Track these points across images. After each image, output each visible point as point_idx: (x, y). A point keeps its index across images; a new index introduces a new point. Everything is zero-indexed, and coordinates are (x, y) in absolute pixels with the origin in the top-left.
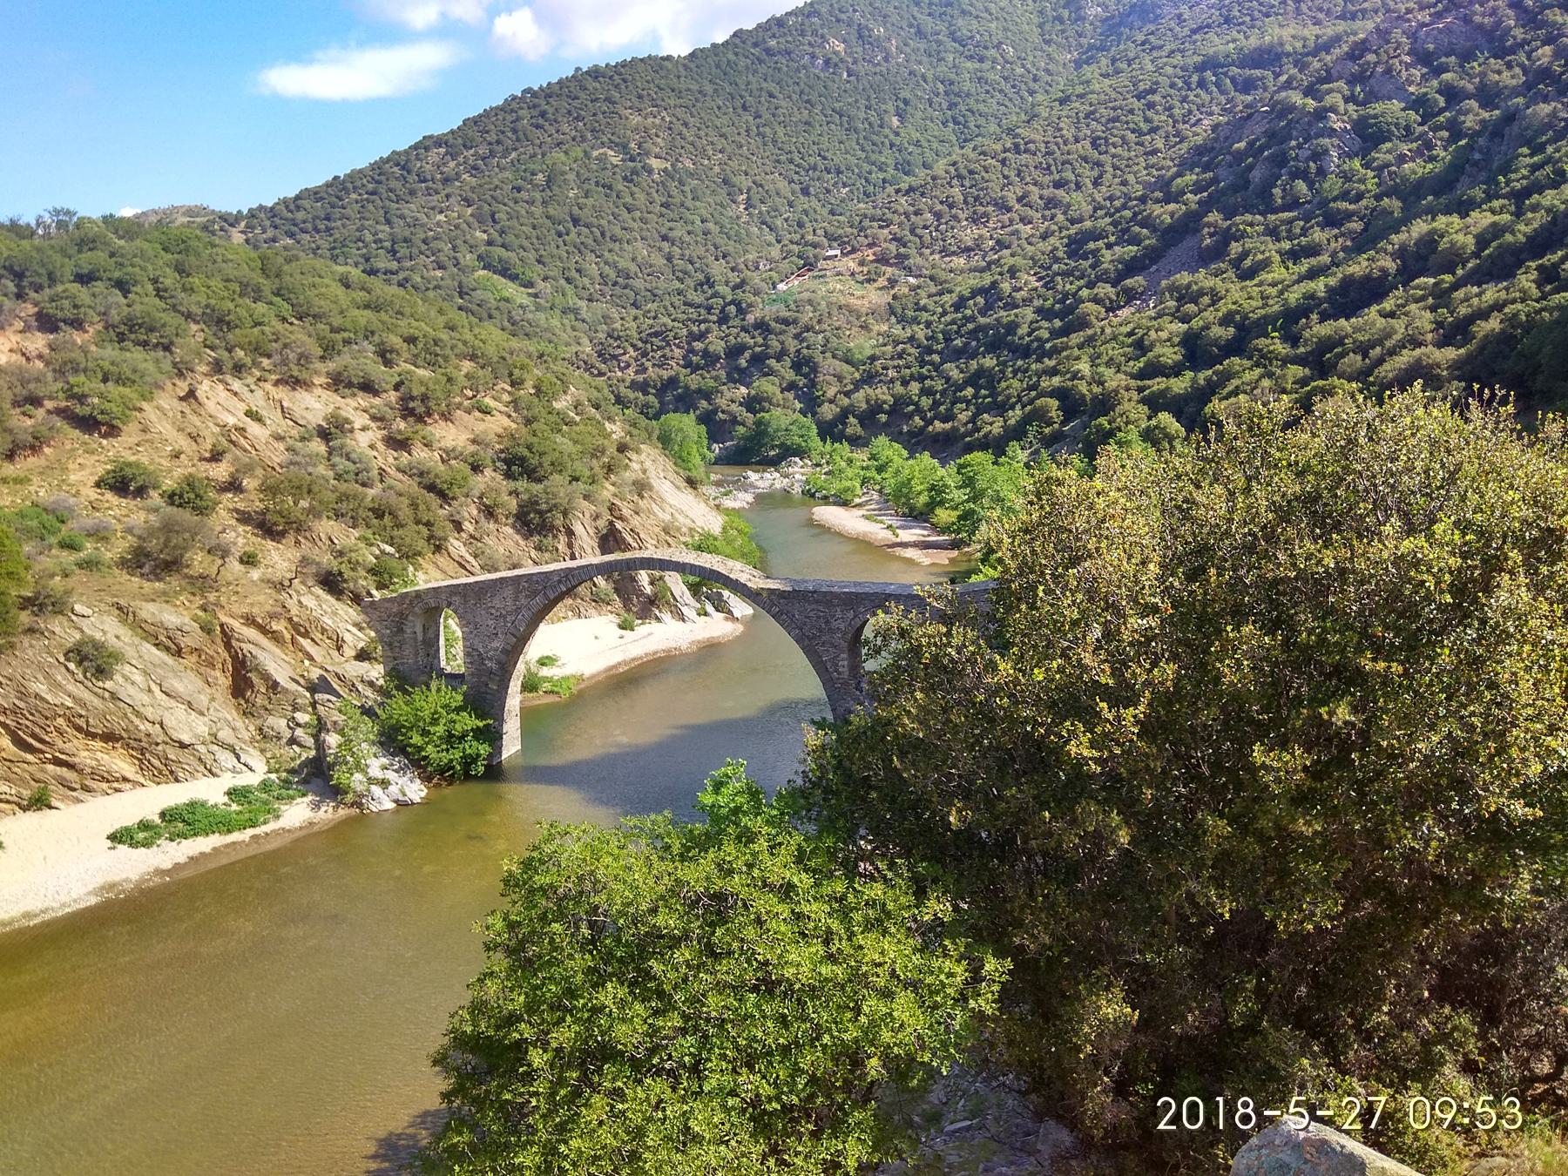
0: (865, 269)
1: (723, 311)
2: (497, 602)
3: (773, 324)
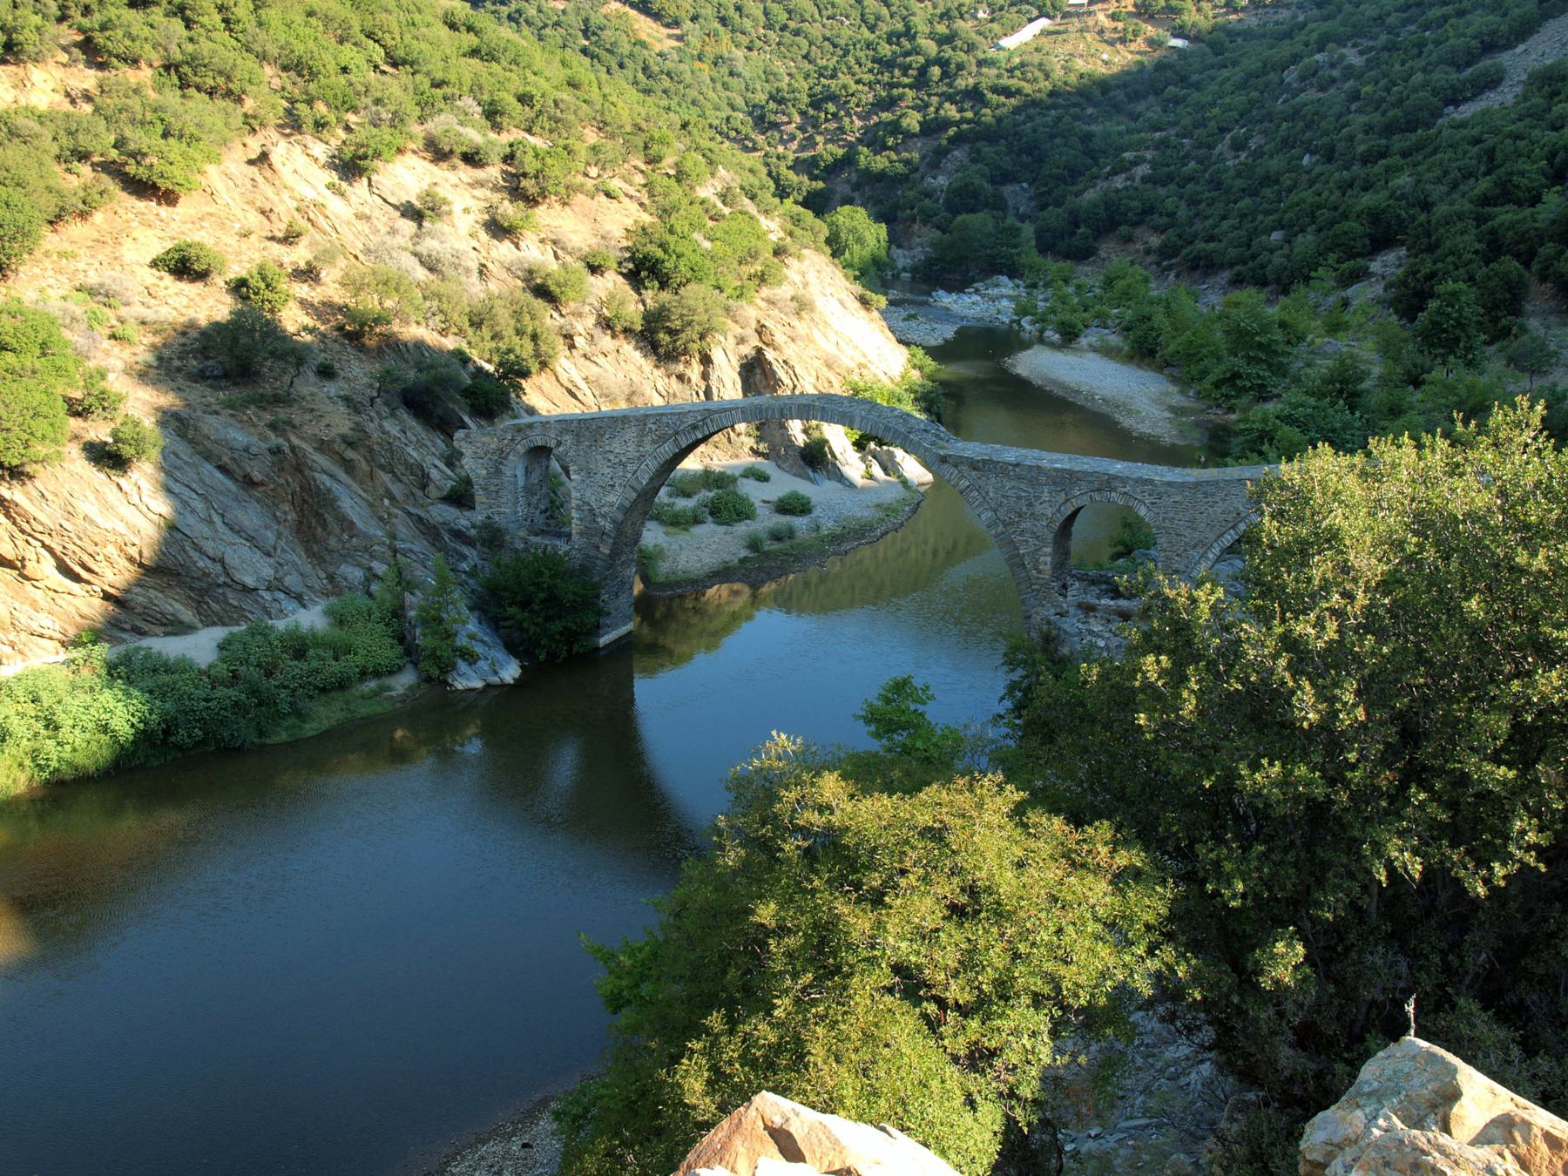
0: (1120, 25)
1: (923, 71)
2: (616, 446)
3: (989, 95)
